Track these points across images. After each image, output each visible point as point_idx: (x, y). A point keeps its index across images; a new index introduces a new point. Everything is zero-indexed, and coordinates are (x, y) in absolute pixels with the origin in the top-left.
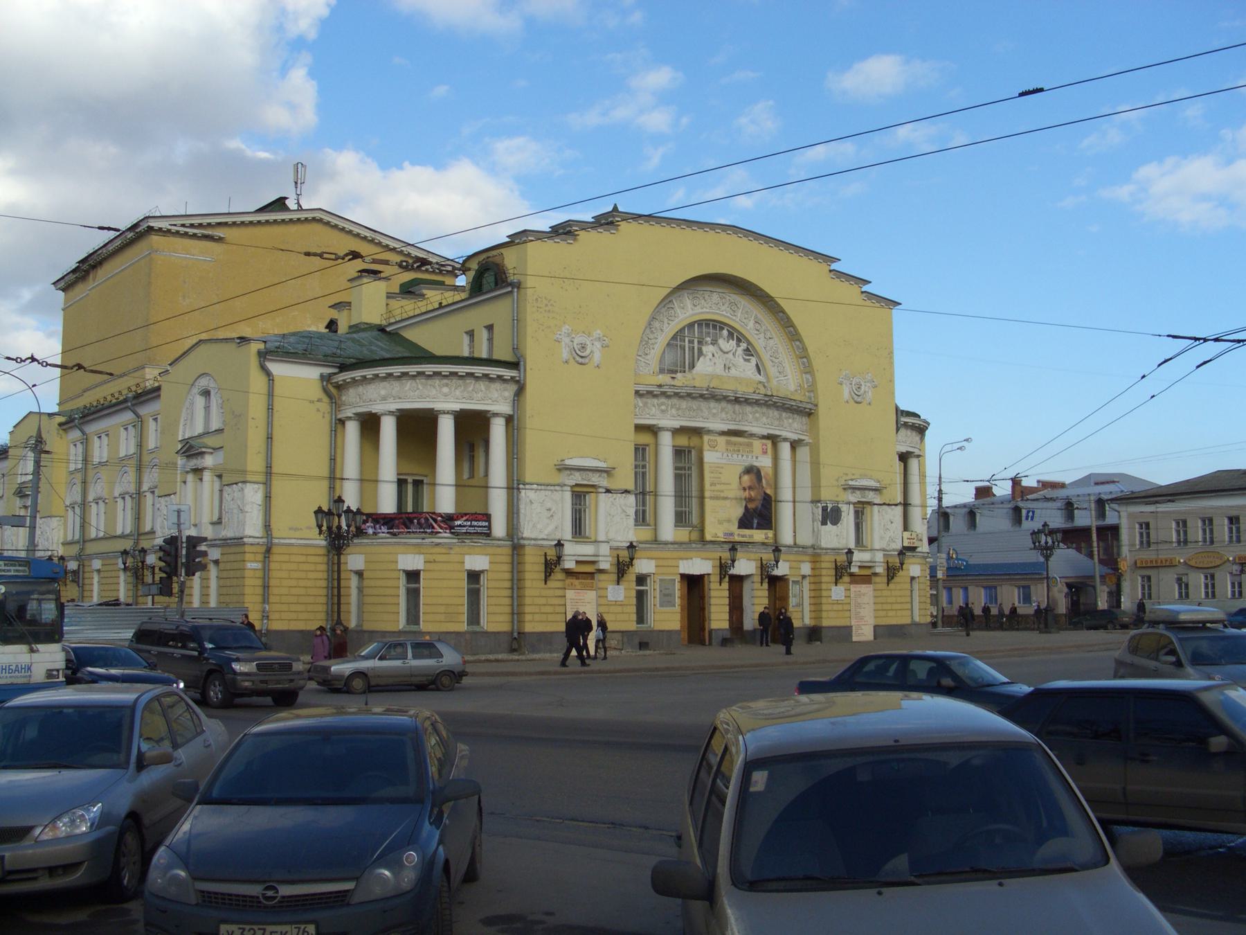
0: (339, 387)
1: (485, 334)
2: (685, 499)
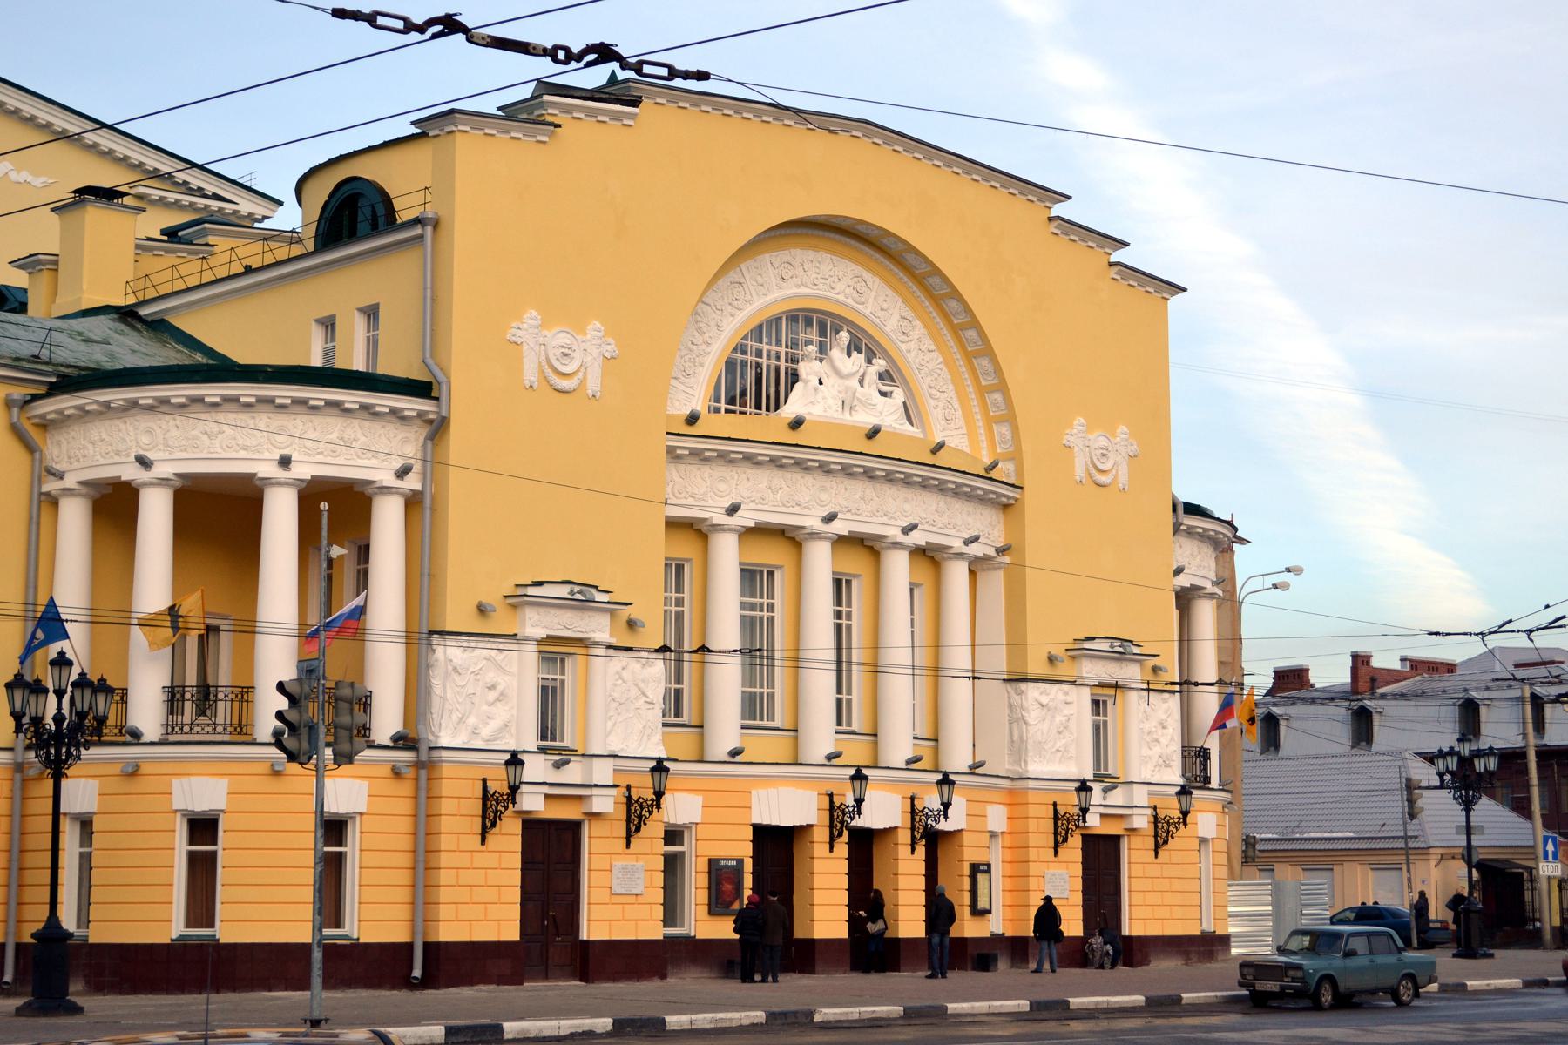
1: (360, 323)
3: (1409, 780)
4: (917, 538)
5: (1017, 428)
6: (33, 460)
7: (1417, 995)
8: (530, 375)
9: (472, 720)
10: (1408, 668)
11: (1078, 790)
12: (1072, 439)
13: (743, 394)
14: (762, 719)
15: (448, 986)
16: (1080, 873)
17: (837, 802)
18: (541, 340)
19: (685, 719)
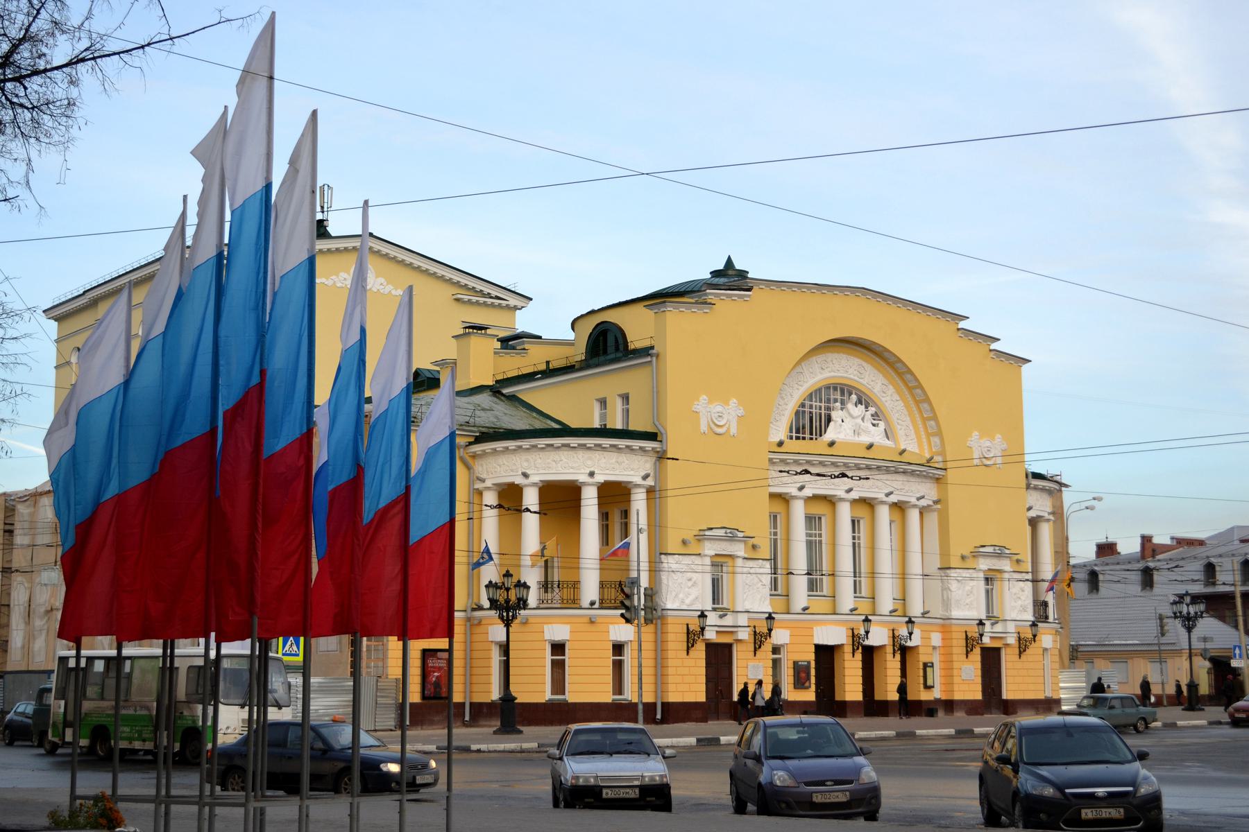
0: (474, 456)
1: (619, 403)
3: (1160, 615)
4: (893, 499)
5: (943, 439)
6: (470, 473)
7: (1147, 727)
8: (704, 427)
9: (681, 596)
10: (1175, 543)
11: (978, 624)
12: (971, 443)
13: (804, 427)
14: (817, 591)
15: (673, 723)
16: (980, 667)
17: (856, 633)
18: (708, 410)
19: (779, 592)
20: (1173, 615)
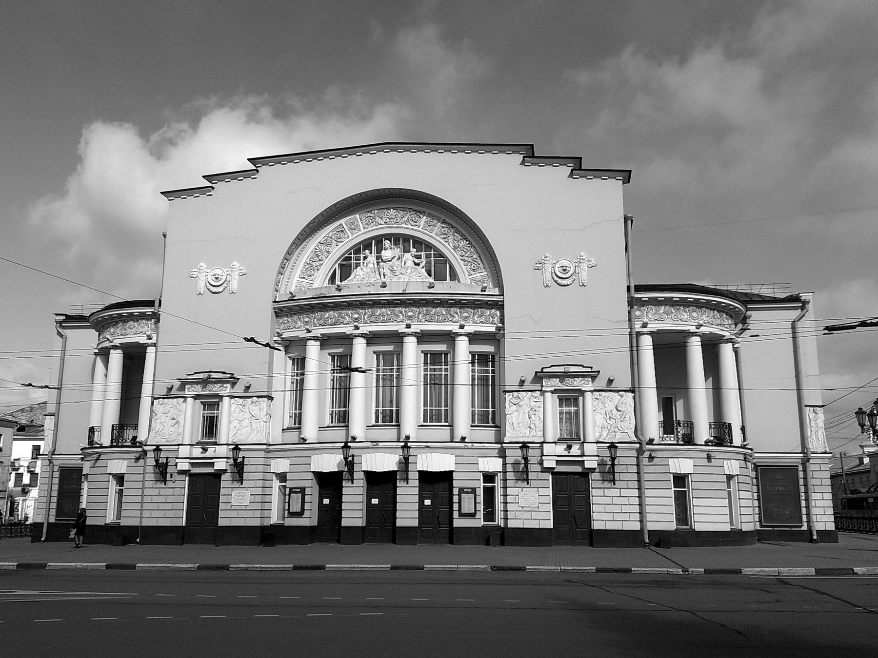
2: (446, 389)
20: (743, 459)
